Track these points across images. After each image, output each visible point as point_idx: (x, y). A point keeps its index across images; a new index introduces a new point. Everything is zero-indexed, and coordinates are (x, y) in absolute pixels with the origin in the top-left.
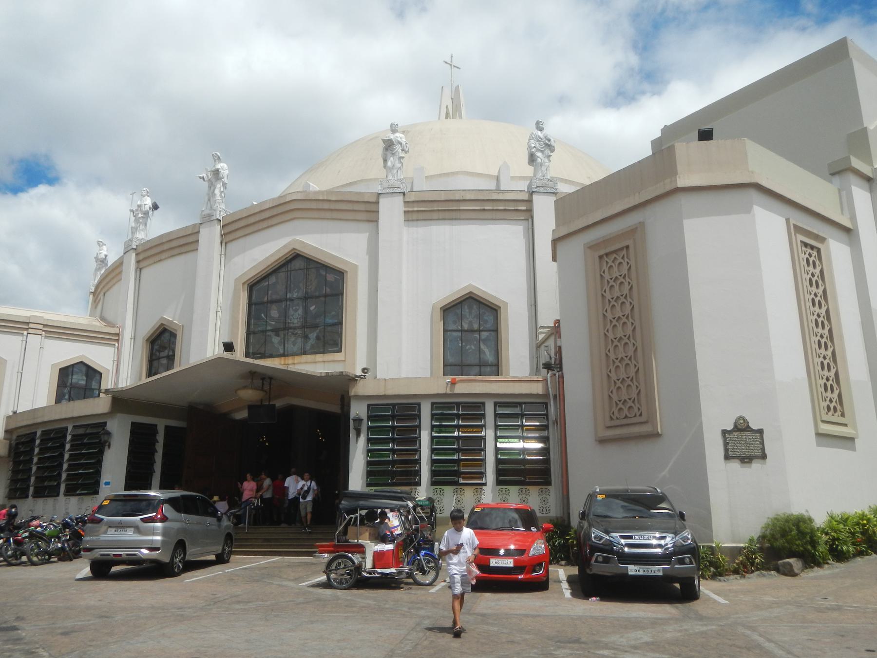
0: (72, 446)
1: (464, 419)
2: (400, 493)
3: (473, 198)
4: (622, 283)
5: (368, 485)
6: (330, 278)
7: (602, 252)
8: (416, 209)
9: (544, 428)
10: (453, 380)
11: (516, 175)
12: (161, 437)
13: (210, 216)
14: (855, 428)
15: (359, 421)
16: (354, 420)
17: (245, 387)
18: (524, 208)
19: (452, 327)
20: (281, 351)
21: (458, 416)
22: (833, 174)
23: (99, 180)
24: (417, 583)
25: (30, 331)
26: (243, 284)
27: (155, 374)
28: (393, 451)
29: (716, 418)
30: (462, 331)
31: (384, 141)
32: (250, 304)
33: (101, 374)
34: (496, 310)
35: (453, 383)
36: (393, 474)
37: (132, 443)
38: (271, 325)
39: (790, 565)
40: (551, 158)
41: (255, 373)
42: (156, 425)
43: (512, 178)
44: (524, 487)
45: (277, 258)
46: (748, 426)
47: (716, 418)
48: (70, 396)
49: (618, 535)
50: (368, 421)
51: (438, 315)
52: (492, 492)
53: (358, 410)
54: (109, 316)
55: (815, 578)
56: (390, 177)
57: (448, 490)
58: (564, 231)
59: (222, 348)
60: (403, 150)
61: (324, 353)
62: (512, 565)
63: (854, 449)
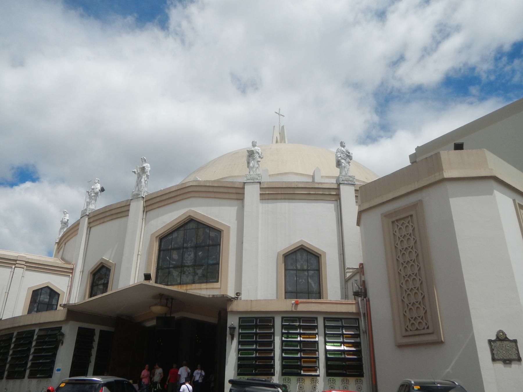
0: (37, 343)
1: (303, 329)
2: (265, 381)
3: (303, 186)
4: (408, 239)
5: (239, 374)
6: (212, 234)
7: (394, 219)
8: (267, 192)
9: (357, 336)
10: (296, 301)
11: (327, 173)
12: (96, 338)
13: (138, 195)
15: (233, 329)
16: (230, 328)
17: (156, 305)
18: (335, 193)
19: (290, 267)
20: (179, 281)
21: (300, 327)
23: (62, 180)
25: (17, 265)
26: (156, 237)
27: (94, 296)
28: (256, 350)
29: (483, 332)
30: (297, 270)
31: (248, 151)
32: (160, 251)
33: (59, 295)
34: (318, 257)
35: (297, 304)
36: (256, 367)
37: (78, 342)
38: (172, 264)
40: (350, 164)
41: (163, 295)
42: (94, 330)
43: (322, 177)
44: (345, 378)
45: (179, 221)
46: (506, 338)
47: (483, 332)
48: (38, 309)
50: (239, 329)
52: (324, 381)
53: (233, 321)
54: (67, 258)
57: (294, 379)
58: (366, 206)
59: (143, 277)
60: (259, 157)
61: (207, 282)
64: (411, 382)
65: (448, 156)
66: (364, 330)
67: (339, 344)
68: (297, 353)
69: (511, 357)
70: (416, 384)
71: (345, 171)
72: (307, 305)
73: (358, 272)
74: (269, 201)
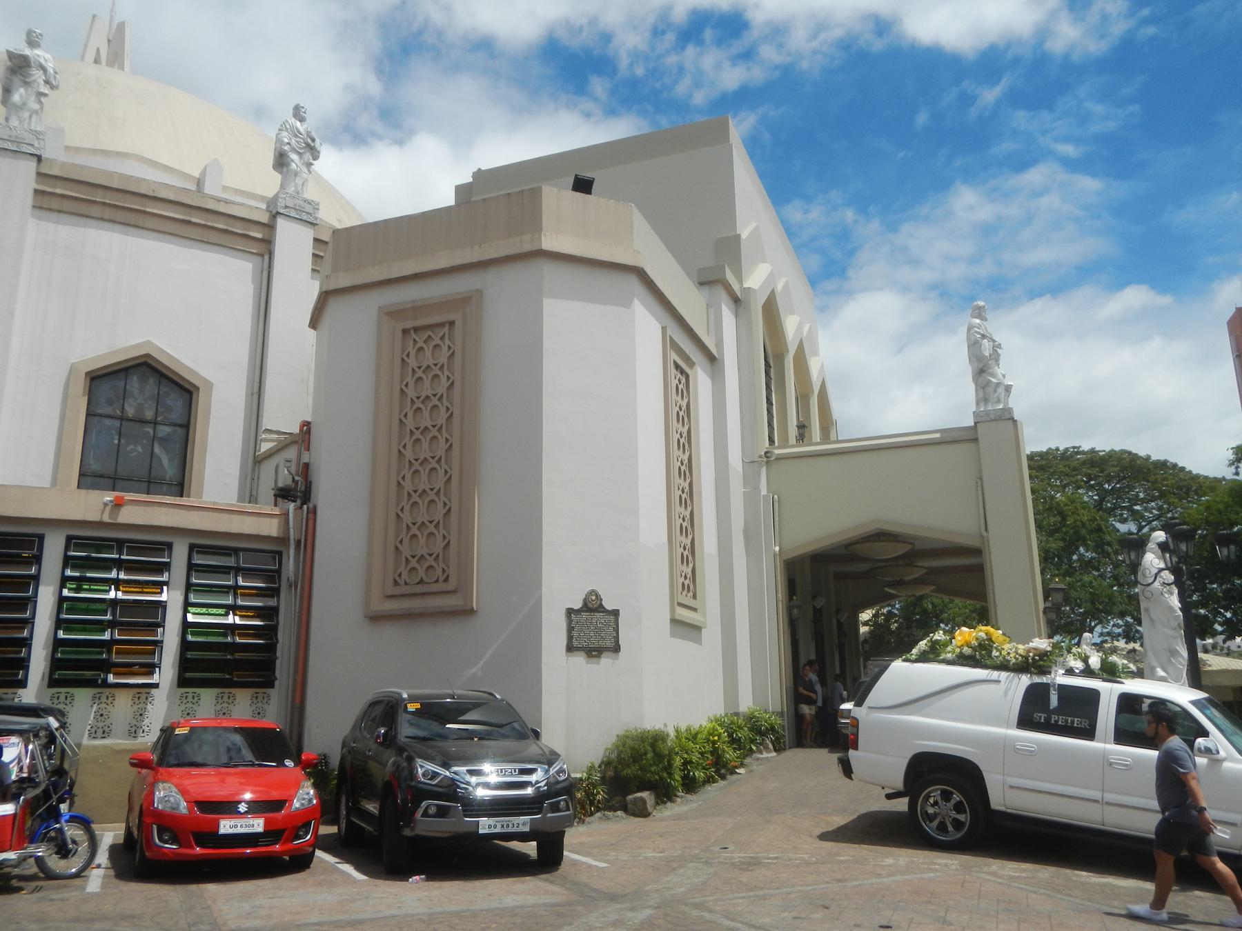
3: (172, 197)
7: (409, 324)
8: (59, 191)
10: (117, 498)
11: (246, 179)
14: (704, 615)
18: (259, 236)
21: (119, 564)
22: (701, 284)
24: (50, 876)
29: (560, 592)
31: (11, 55)
34: (190, 393)
35: (118, 504)
39: (643, 801)
47: (560, 592)
49: (464, 769)
51: (80, 385)
52: (169, 697)
55: (678, 818)
56: (14, 122)
57: (82, 696)
58: (344, 281)
62: (260, 829)
63: (699, 642)
64: (400, 695)
65: (558, 200)
66: (292, 578)
67: (221, 611)
68: (104, 631)
69: (602, 644)
70: (412, 699)
71: (296, 185)
72: (149, 509)
73: (295, 442)
74: (63, 217)
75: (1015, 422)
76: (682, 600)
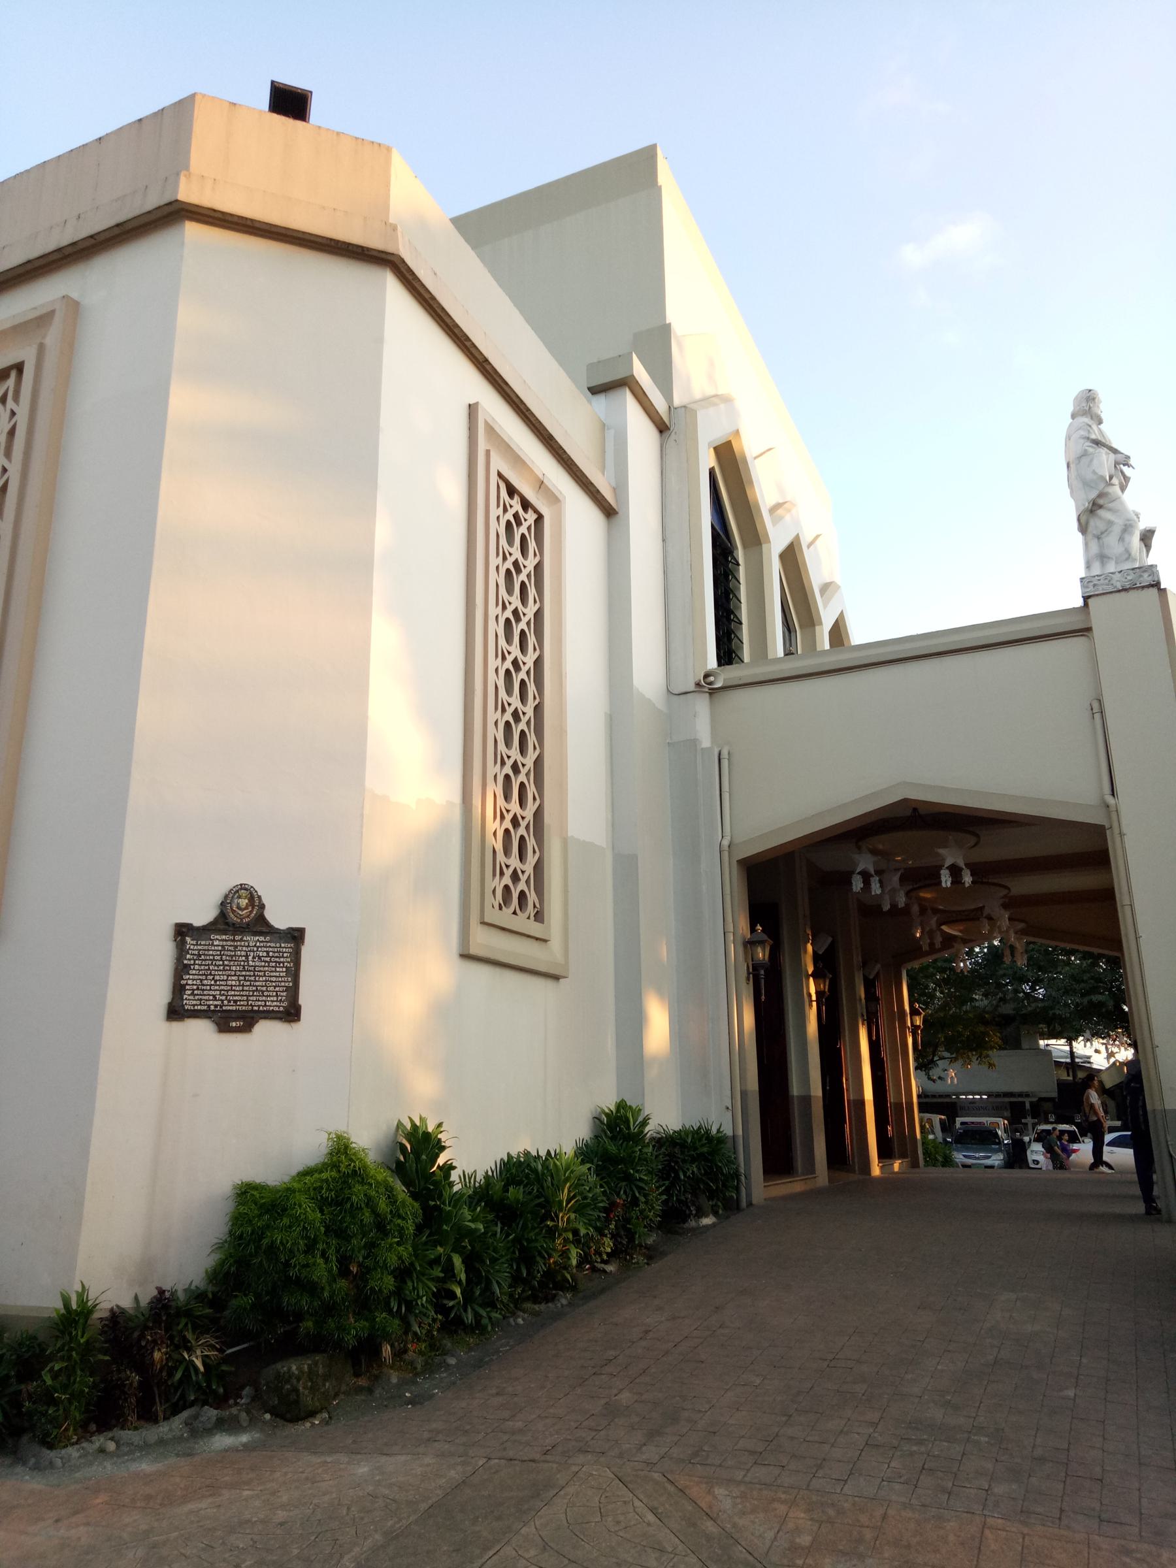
46: (261, 919)
69: (258, 1004)
75: (1163, 592)
76: (493, 916)
